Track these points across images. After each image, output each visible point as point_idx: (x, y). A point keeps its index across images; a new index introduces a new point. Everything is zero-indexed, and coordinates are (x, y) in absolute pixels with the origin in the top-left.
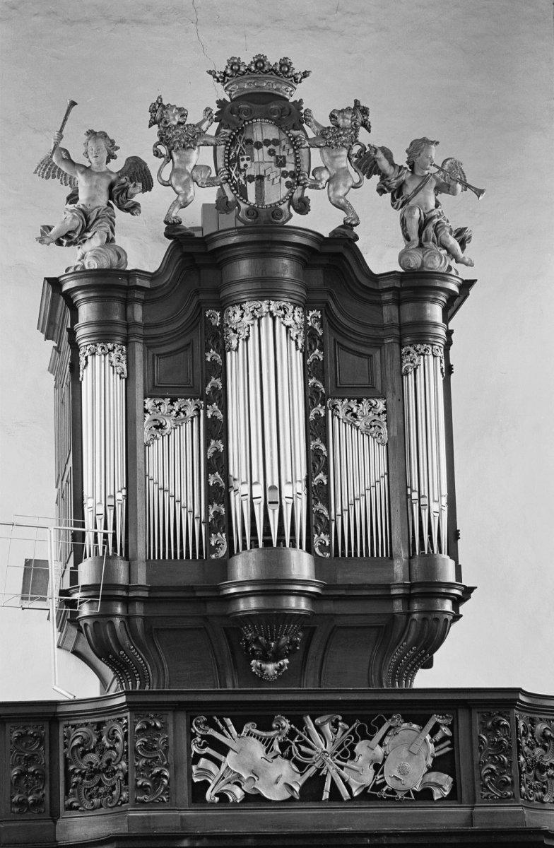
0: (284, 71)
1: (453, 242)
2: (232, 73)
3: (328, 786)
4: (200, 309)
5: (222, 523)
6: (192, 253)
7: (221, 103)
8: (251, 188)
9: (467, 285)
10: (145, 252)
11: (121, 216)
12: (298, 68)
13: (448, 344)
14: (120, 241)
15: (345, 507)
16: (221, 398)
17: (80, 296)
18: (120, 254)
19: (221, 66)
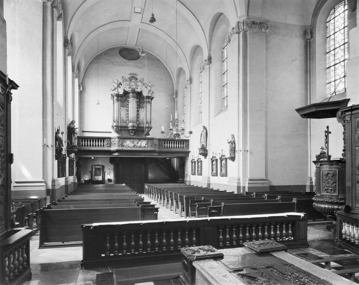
0: (135, 74)
3: (214, 249)
6: (126, 93)
7: (129, 77)
8: (132, 86)
9: (153, 98)
10: (121, 92)
11: (119, 88)
13: (151, 103)
15: (134, 117)
16: (128, 107)
17: (114, 96)
18: (119, 92)
19: (129, 73)
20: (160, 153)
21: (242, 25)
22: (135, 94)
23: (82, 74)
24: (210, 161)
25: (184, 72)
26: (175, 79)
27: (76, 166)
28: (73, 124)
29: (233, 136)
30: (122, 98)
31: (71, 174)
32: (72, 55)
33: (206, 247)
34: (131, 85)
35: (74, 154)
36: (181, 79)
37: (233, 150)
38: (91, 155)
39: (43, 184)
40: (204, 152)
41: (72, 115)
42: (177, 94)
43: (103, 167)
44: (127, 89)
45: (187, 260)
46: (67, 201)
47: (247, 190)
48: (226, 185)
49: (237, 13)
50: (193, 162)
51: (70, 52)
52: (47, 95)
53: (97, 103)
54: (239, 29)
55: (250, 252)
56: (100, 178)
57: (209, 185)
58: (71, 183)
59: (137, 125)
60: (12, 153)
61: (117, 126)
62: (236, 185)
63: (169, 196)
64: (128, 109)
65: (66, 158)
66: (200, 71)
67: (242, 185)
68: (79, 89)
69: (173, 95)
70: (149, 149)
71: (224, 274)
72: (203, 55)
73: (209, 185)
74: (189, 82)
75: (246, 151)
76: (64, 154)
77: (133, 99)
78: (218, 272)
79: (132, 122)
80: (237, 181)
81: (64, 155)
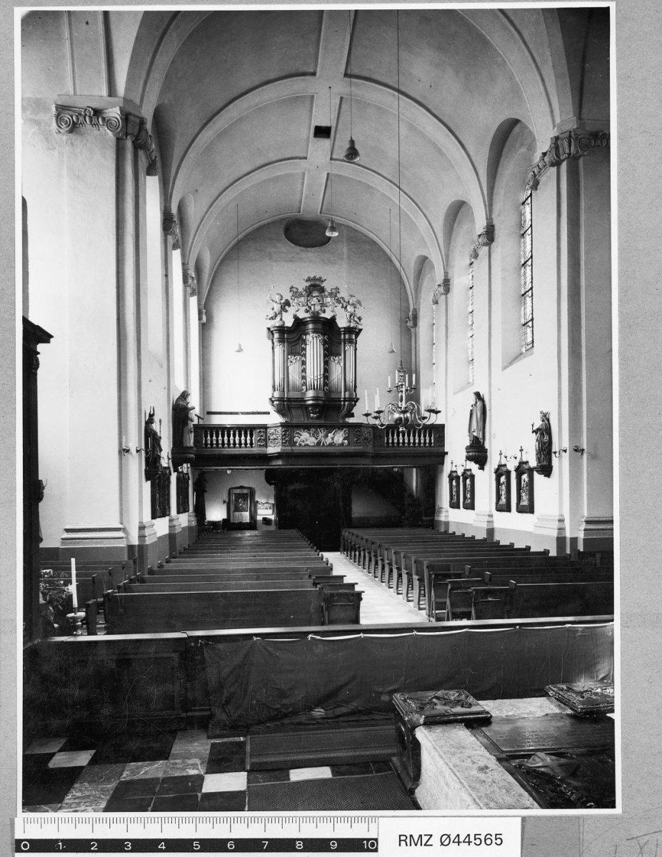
0: (320, 279)
1: (358, 320)
2: (308, 280)
3: (471, 699)
4: (301, 336)
5: (305, 384)
6: (299, 323)
8: (312, 307)
9: (360, 330)
10: (289, 322)
11: (283, 313)
12: (323, 278)
14: (283, 319)
15: (319, 377)
16: (305, 355)
18: (284, 323)
19: (306, 278)
20: (377, 457)
21: (566, 144)
22: (320, 325)
23: (204, 288)
24: (494, 476)
25: (432, 267)
26: (412, 283)
27: (194, 490)
28: (185, 399)
29: (545, 418)
30: (291, 337)
31: (182, 508)
32: (183, 245)
33: (453, 695)
34: (310, 305)
35: (189, 465)
36: (426, 283)
37: (545, 450)
38: (226, 466)
39: (120, 534)
40: (478, 452)
41: (184, 379)
42: (415, 318)
43: (252, 493)
44: (302, 315)
45: (404, 723)
46: (168, 572)
47: (581, 548)
48: (531, 533)
49: (552, 116)
50: (453, 476)
51: (177, 241)
52: (126, 340)
53: (237, 348)
54: (558, 155)
55: (557, 711)
56: (246, 517)
57: (491, 532)
58: (160, 538)
59: (325, 393)
60: (40, 479)
61: (281, 399)
62: (555, 534)
63: (394, 559)
64: (303, 359)
65: (170, 474)
66: (469, 262)
67: (568, 535)
68: (200, 319)
69: (407, 322)
70: (352, 449)
71: (482, 764)
72: (473, 221)
73: (491, 532)
74: (441, 289)
75: (578, 450)
76: (166, 465)
77: (315, 335)
78: (469, 757)
79: (314, 389)
80: (556, 525)
81: (165, 468)
